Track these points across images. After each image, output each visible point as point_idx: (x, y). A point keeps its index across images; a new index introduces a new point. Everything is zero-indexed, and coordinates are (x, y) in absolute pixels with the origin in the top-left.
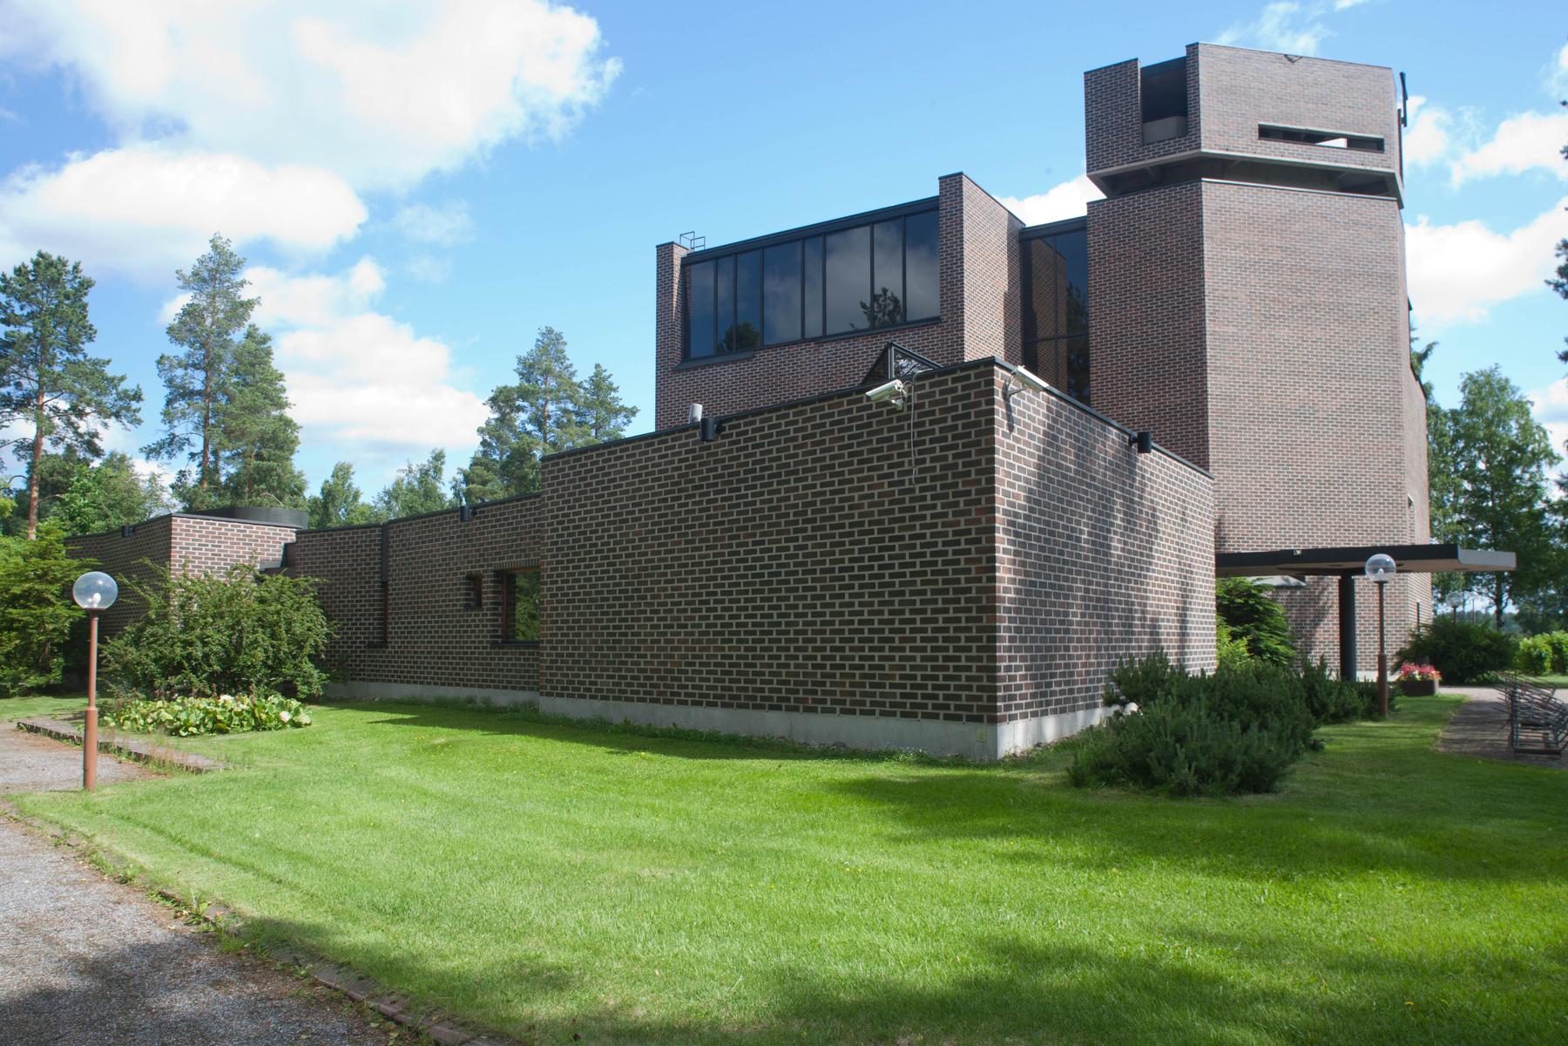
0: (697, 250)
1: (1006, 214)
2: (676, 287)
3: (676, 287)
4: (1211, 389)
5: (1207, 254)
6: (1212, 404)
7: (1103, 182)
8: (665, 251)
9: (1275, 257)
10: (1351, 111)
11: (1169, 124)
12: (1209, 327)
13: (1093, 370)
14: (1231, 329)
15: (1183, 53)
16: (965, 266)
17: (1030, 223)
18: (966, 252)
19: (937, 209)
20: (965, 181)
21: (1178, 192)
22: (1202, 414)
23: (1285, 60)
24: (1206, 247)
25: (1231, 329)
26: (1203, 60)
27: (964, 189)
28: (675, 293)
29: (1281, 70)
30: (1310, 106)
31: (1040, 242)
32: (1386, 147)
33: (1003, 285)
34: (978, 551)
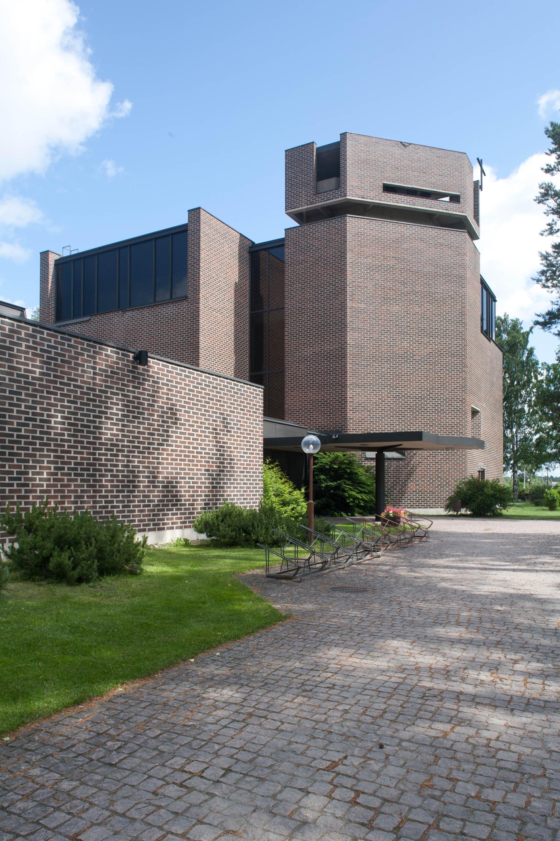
0: (73, 253)
1: (239, 236)
2: (50, 278)
3: (50, 278)
4: (349, 341)
5: (349, 260)
6: (350, 350)
7: (298, 216)
8: (44, 255)
9: (392, 262)
10: (441, 177)
11: (332, 181)
12: (349, 304)
13: (286, 329)
14: (362, 306)
15: (338, 139)
16: (201, 265)
17: (258, 240)
18: (202, 256)
19: (186, 231)
20: (202, 213)
21: (334, 222)
22: (343, 356)
23: (400, 145)
24: (349, 255)
25: (362, 306)
26: (349, 142)
27: (202, 218)
28: (50, 281)
29: (398, 151)
30: (415, 173)
31: (264, 252)
32: (461, 200)
33: (235, 277)
34: (88, 475)
